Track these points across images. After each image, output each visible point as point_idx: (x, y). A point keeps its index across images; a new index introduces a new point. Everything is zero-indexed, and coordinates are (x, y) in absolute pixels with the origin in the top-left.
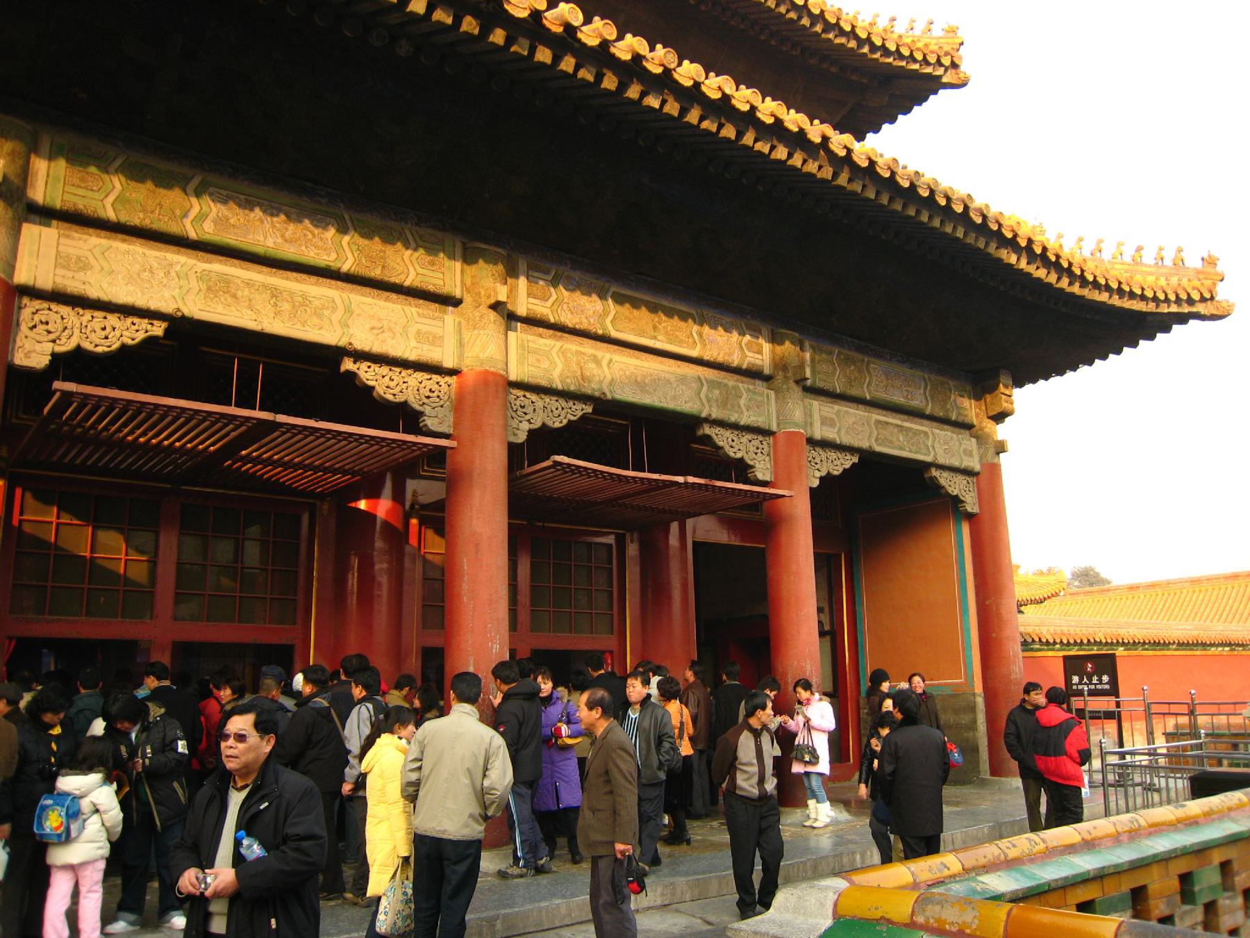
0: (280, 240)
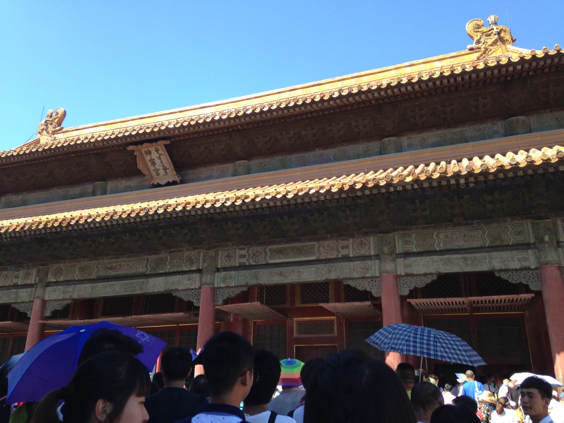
0: (464, 242)
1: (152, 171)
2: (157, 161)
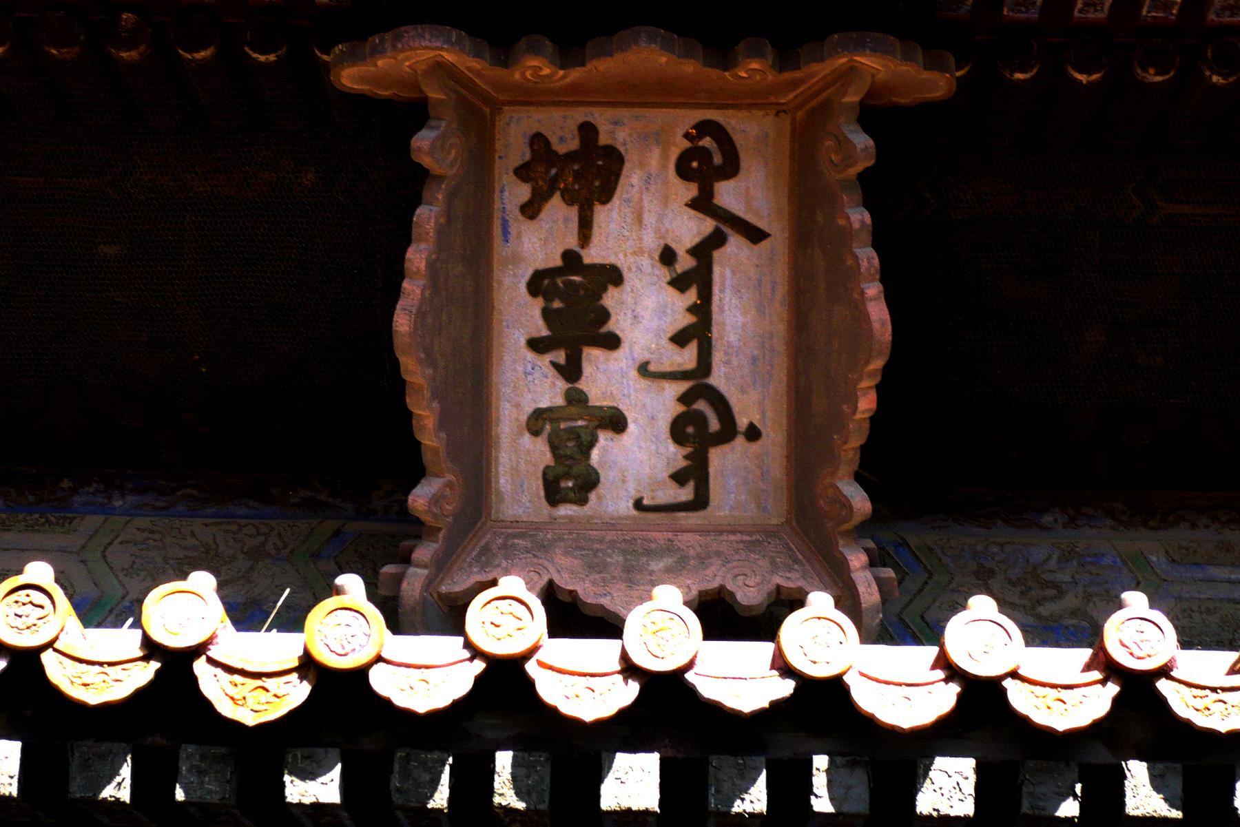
1: (509, 416)
2: (646, 312)
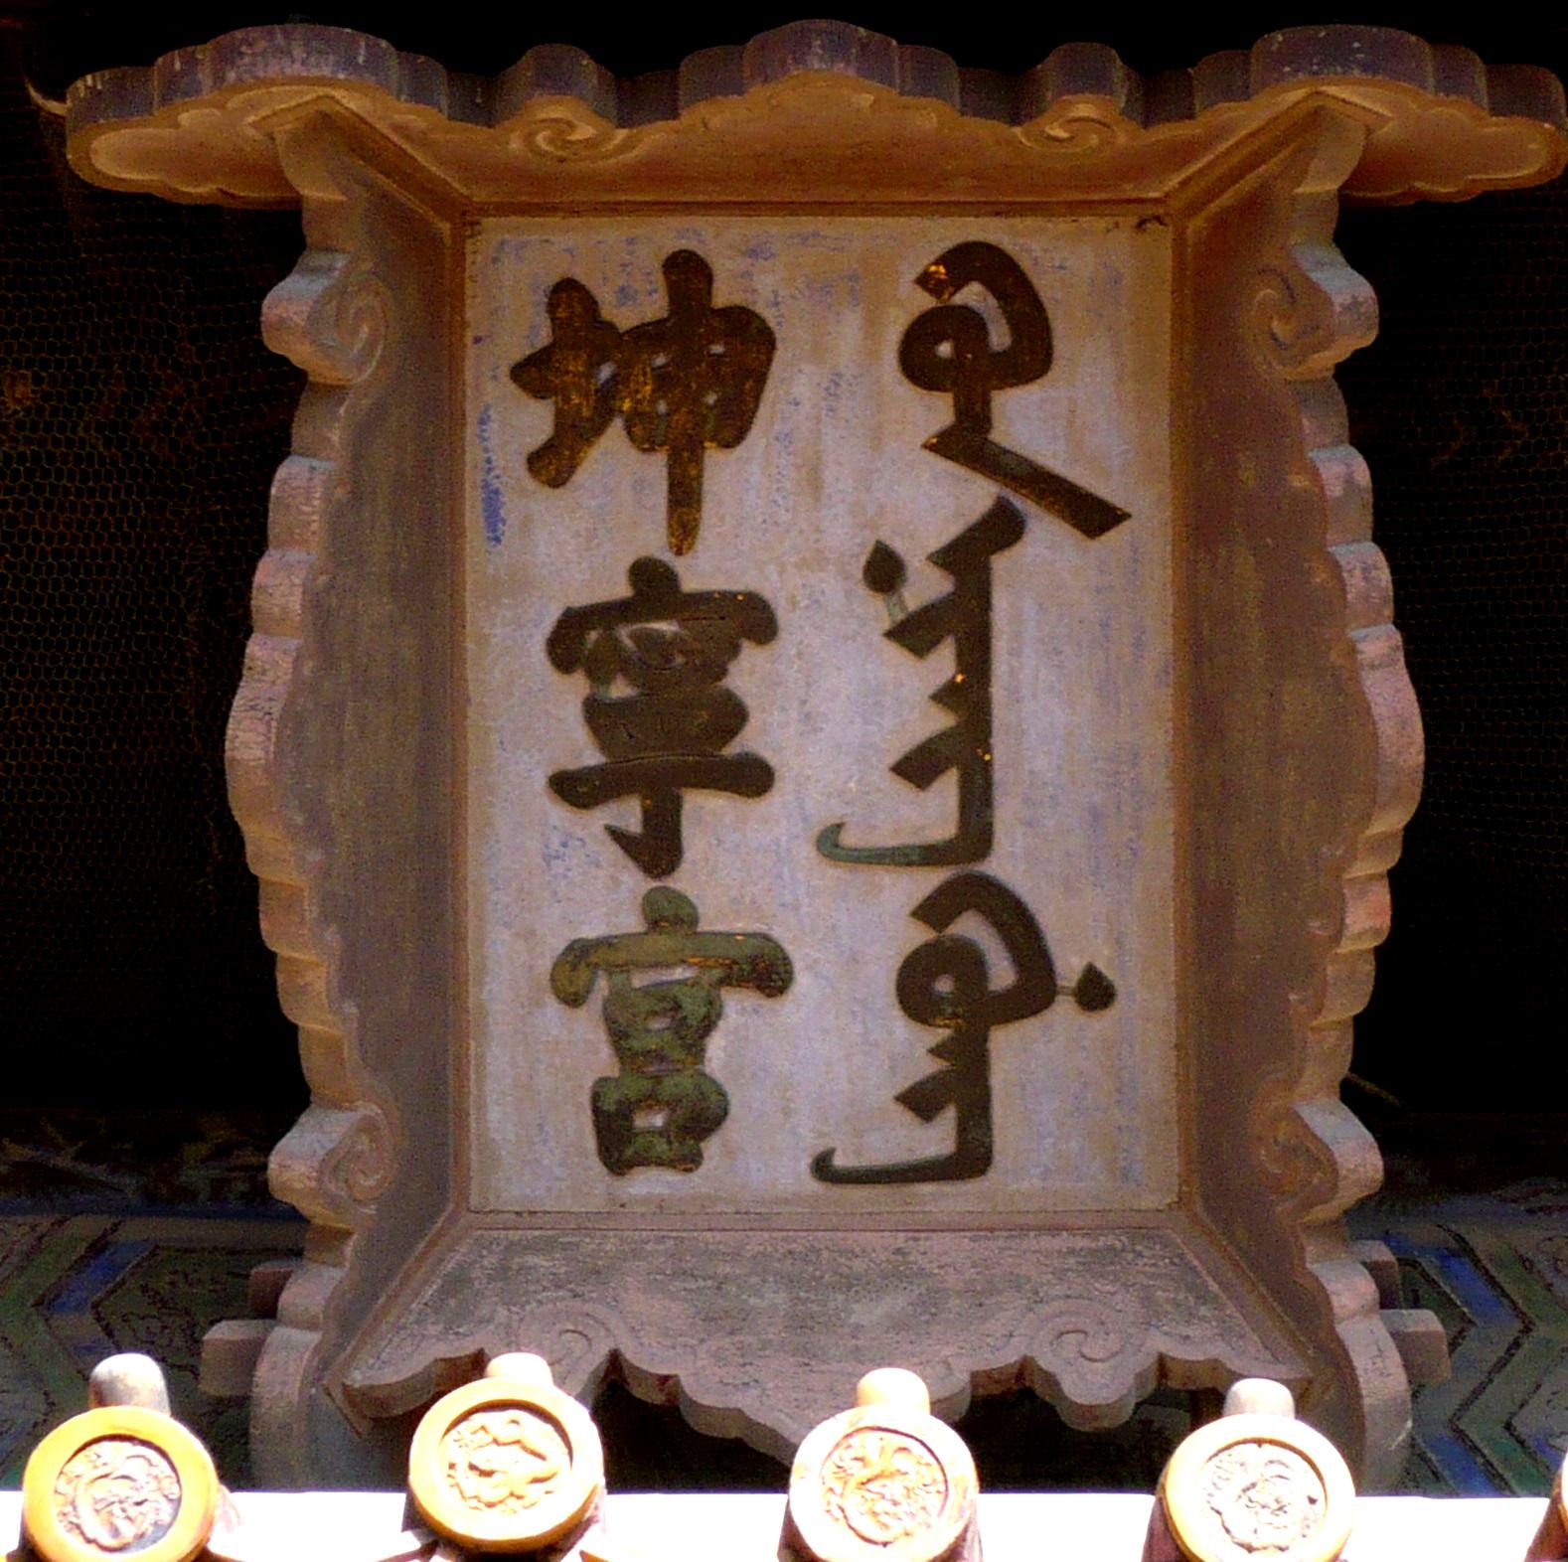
2: (833, 704)
